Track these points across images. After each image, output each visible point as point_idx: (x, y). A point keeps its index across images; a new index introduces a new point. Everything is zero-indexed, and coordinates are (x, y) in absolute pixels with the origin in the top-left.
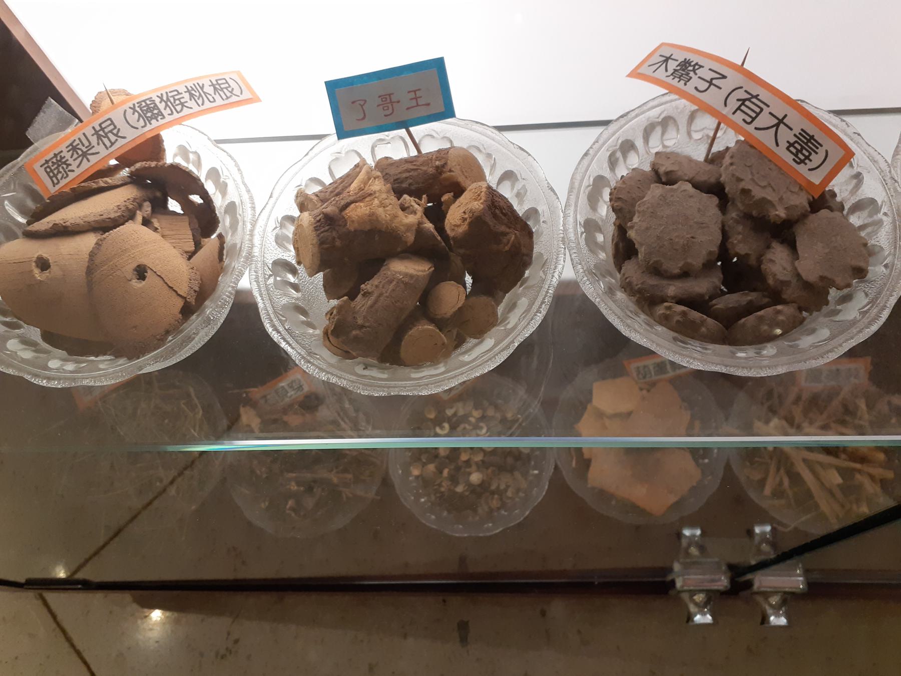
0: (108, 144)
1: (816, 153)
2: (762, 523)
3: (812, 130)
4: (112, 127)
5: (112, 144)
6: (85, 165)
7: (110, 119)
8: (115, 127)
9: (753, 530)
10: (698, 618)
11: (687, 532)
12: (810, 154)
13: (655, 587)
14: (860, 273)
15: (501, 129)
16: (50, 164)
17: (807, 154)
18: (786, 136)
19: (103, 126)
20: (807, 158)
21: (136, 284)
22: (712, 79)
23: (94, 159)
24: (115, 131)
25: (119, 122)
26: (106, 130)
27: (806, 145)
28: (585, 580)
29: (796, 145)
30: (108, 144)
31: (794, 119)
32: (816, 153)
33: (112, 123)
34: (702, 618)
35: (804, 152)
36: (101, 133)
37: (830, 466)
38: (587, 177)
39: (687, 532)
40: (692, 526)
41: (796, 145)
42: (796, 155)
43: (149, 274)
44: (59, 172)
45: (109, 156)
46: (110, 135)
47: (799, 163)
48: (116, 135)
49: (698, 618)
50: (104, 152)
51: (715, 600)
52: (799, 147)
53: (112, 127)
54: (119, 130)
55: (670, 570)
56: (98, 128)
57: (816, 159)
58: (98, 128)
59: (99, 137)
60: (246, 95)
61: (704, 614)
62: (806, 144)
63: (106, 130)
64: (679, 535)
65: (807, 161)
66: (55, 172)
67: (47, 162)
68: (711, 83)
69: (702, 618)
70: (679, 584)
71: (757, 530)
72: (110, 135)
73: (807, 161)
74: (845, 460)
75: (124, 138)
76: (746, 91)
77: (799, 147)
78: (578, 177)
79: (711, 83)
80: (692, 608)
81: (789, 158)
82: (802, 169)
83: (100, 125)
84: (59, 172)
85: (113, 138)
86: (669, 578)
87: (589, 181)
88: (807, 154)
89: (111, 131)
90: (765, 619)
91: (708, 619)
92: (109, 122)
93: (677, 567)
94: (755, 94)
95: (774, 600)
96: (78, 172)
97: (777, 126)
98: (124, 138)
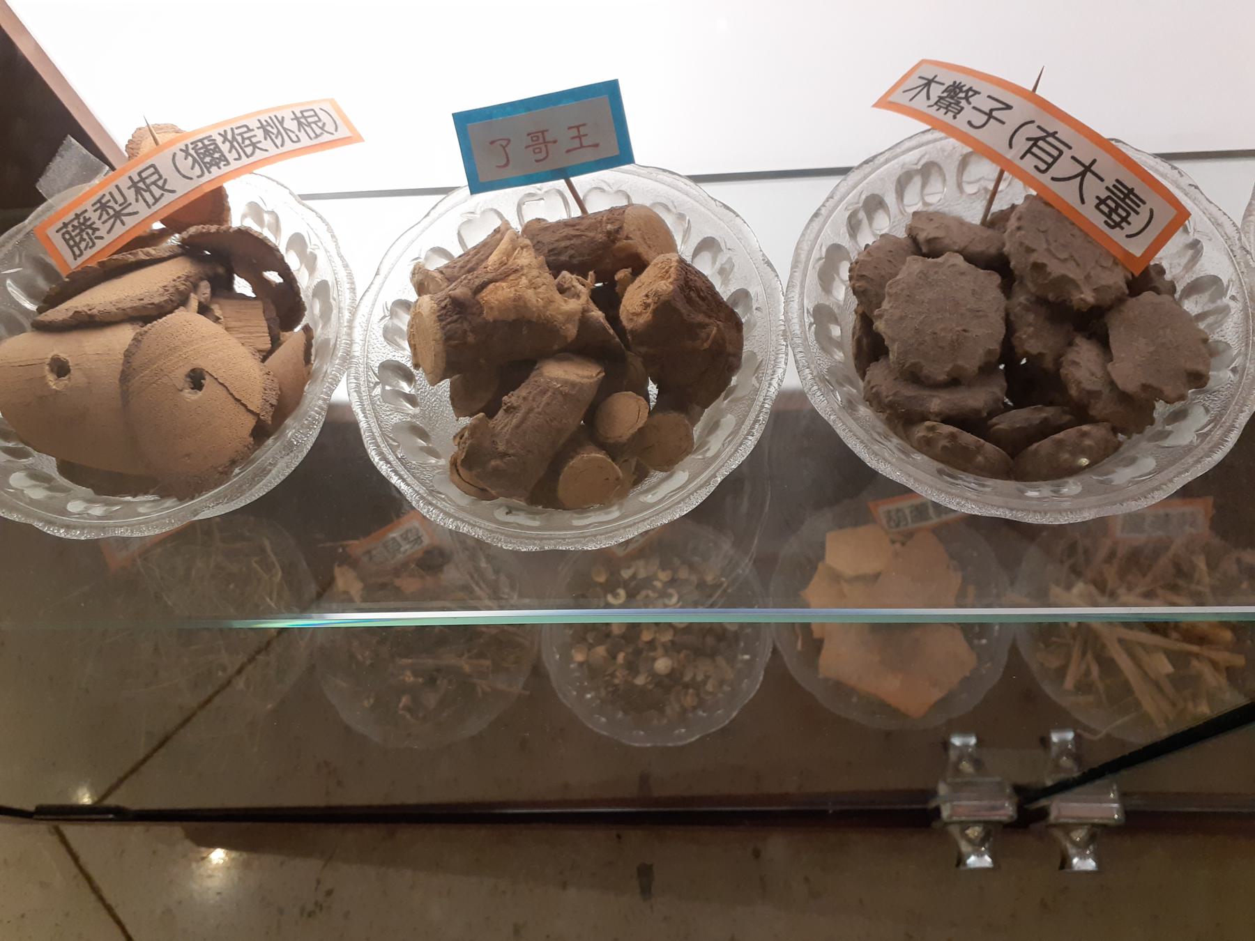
0: (151, 200)
1: (1137, 213)
2: (1062, 727)
3: (1131, 181)
4: (156, 177)
5: (156, 200)
6: (119, 230)
7: (153, 166)
8: (161, 177)
9: (1050, 738)
10: (972, 861)
11: (957, 741)
12: (1129, 214)
13: (913, 817)
14: (1198, 380)
15: (697, 179)
16: (70, 228)
17: (1124, 214)
18: (1095, 190)
19: (144, 175)
20: (1124, 219)
21: (189, 395)
22: (991, 110)
23: (130, 222)
24: (160, 183)
25: (166, 170)
26: (148, 181)
27: (1122, 201)
28: (815, 808)
29: (1109, 202)
30: (151, 200)
31: (1105, 165)
32: (1137, 213)
33: (157, 171)
34: (978, 861)
35: (1120, 211)
36: (141, 185)
37: (1157, 648)
38: (817, 247)
39: (957, 741)
40: (964, 732)
41: (1109, 202)
42: (1109, 216)
43: (207, 382)
44: (83, 239)
45: (152, 218)
46: (153, 188)
47: (1112, 227)
48: (162, 188)
49: (972, 861)
50: (144, 212)
51: (995, 835)
52: (1113, 205)
53: (156, 177)
54: (165, 181)
55: (933, 793)
56: (136, 178)
57: (1137, 221)
58: (136, 178)
59: (138, 191)
60: (343, 132)
61: (980, 855)
62: (1123, 200)
63: (148, 181)
64: (946, 745)
65: (1124, 224)
66: (77, 239)
67: (65, 225)
68: (990, 115)
69: (978, 861)
70: (946, 813)
71: (1055, 738)
72: (153, 188)
73: (1124, 224)
74: (1177, 640)
75: (173, 191)
76: (1039, 127)
77: (1113, 205)
78: (806, 246)
79: (990, 115)
80: (965, 847)
81: (1098, 220)
82: (1117, 235)
83: (139, 174)
84: (83, 239)
85: (157, 192)
86: (932, 805)
87: (820, 251)
88: (1124, 214)
89: (154, 183)
90: (1065, 862)
91: (987, 861)
92: (152, 170)
93: (943, 789)
94: (1051, 131)
95: (1078, 836)
96: (108, 239)
97: (1082, 175)
98: (173, 191)
